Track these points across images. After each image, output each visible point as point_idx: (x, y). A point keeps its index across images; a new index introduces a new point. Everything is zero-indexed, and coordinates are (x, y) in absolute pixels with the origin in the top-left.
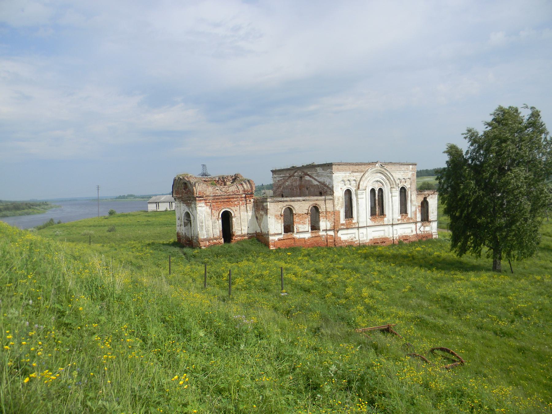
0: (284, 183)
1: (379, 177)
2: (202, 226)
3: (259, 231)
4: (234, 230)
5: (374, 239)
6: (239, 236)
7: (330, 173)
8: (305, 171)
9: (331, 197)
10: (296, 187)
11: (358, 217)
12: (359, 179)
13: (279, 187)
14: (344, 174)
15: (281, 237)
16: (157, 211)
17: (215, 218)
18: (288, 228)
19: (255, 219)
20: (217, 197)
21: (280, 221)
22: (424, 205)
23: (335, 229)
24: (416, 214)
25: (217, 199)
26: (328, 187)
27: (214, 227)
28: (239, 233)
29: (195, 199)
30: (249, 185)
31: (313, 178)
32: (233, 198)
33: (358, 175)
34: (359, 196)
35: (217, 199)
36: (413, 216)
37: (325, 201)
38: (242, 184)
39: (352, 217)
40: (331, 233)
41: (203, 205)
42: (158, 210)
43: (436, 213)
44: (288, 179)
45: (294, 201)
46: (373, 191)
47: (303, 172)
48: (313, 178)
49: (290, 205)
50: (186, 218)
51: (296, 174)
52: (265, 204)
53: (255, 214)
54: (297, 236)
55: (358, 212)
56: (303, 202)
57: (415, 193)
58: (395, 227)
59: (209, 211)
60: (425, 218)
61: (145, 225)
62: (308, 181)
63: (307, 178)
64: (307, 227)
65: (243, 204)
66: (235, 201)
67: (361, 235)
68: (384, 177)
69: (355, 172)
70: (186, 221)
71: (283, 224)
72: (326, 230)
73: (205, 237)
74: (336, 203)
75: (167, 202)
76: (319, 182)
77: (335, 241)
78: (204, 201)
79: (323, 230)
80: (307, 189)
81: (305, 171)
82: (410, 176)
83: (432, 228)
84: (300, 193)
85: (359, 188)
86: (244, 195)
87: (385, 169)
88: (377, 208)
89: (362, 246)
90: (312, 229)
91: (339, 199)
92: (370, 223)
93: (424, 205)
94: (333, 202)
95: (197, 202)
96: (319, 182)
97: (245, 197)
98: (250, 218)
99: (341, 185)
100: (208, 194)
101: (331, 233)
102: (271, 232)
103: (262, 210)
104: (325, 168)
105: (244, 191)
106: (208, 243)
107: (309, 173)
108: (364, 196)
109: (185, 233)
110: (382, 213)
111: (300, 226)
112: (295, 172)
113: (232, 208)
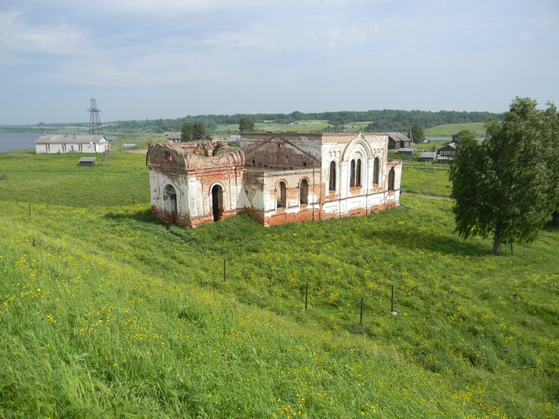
1: (359, 148)
2: (194, 203)
3: (249, 205)
4: (224, 206)
5: (352, 211)
6: (229, 211)
7: (318, 144)
8: (286, 138)
9: (318, 170)
10: (272, 154)
11: (340, 189)
12: (343, 151)
13: (251, 151)
14: (331, 146)
15: (274, 213)
16: (47, 154)
18: (281, 204)
19: (245, 193)
20: (208, 170)
22: (392, 173)
23: (321, 202)
24: (385, 184)
25: (209, 172)
26: (314, 158)
29: (185, 173)
30: (239, 157)
31: (295, 147)
32: (223, 171)
33: (343, 146)
34: (342, 168)
35: (209, 172)
36: (383, 186)
37: (314, 173)
38: (232, 155)
39: (334, 189)
40: (317, 206)
41: (194, 179)
42: (49, 152)
43: (399, 183)
44: (262, 145)
46: (353, 161)
47: (283, 139)
48: (295, 147)
49: (284, 180)
52: (260, 179)
53: (245, 187)
54: (288, 211)
56: (295, 175)
57: (385, 163)
59: (200, 185)
60: (391, 188)
61: (39, 171)
62: (289, 149)
63: (288, 146)
67: (342, 208)
69: (340, 143)
70: (165, 194)
71: (276, 200)
73: (196, 215)
74: (323, 176)
75: (59, 143)
77: (320, 214)
78: (195, 175)
79: (310, 204)
80: (287, 157)
81: (286, 138)
82: (383, 146)
83: (395, 197)
85: (343, 160)
86: (234, 168)
87: (365, 140)
88: (356, 179)
89: (344, 219)
91: (325, 171)
92: (350, 195)
93: (392, 173)
94: (321, 175)
95: (189, 176)
97: (235, 170)
98: (239, 192)
99: (328, 156)
100: (199, 166)
101: (317, 206)
102: (266, 209)
103: (254, 184)
104: (312, 138)
105: (234, 162)
106: (198, 222)
107: (290, 141)
108: (346, 168)
110: (359, 184)
111: (291, 200)
112: (272, 138)
113: (222, 182)
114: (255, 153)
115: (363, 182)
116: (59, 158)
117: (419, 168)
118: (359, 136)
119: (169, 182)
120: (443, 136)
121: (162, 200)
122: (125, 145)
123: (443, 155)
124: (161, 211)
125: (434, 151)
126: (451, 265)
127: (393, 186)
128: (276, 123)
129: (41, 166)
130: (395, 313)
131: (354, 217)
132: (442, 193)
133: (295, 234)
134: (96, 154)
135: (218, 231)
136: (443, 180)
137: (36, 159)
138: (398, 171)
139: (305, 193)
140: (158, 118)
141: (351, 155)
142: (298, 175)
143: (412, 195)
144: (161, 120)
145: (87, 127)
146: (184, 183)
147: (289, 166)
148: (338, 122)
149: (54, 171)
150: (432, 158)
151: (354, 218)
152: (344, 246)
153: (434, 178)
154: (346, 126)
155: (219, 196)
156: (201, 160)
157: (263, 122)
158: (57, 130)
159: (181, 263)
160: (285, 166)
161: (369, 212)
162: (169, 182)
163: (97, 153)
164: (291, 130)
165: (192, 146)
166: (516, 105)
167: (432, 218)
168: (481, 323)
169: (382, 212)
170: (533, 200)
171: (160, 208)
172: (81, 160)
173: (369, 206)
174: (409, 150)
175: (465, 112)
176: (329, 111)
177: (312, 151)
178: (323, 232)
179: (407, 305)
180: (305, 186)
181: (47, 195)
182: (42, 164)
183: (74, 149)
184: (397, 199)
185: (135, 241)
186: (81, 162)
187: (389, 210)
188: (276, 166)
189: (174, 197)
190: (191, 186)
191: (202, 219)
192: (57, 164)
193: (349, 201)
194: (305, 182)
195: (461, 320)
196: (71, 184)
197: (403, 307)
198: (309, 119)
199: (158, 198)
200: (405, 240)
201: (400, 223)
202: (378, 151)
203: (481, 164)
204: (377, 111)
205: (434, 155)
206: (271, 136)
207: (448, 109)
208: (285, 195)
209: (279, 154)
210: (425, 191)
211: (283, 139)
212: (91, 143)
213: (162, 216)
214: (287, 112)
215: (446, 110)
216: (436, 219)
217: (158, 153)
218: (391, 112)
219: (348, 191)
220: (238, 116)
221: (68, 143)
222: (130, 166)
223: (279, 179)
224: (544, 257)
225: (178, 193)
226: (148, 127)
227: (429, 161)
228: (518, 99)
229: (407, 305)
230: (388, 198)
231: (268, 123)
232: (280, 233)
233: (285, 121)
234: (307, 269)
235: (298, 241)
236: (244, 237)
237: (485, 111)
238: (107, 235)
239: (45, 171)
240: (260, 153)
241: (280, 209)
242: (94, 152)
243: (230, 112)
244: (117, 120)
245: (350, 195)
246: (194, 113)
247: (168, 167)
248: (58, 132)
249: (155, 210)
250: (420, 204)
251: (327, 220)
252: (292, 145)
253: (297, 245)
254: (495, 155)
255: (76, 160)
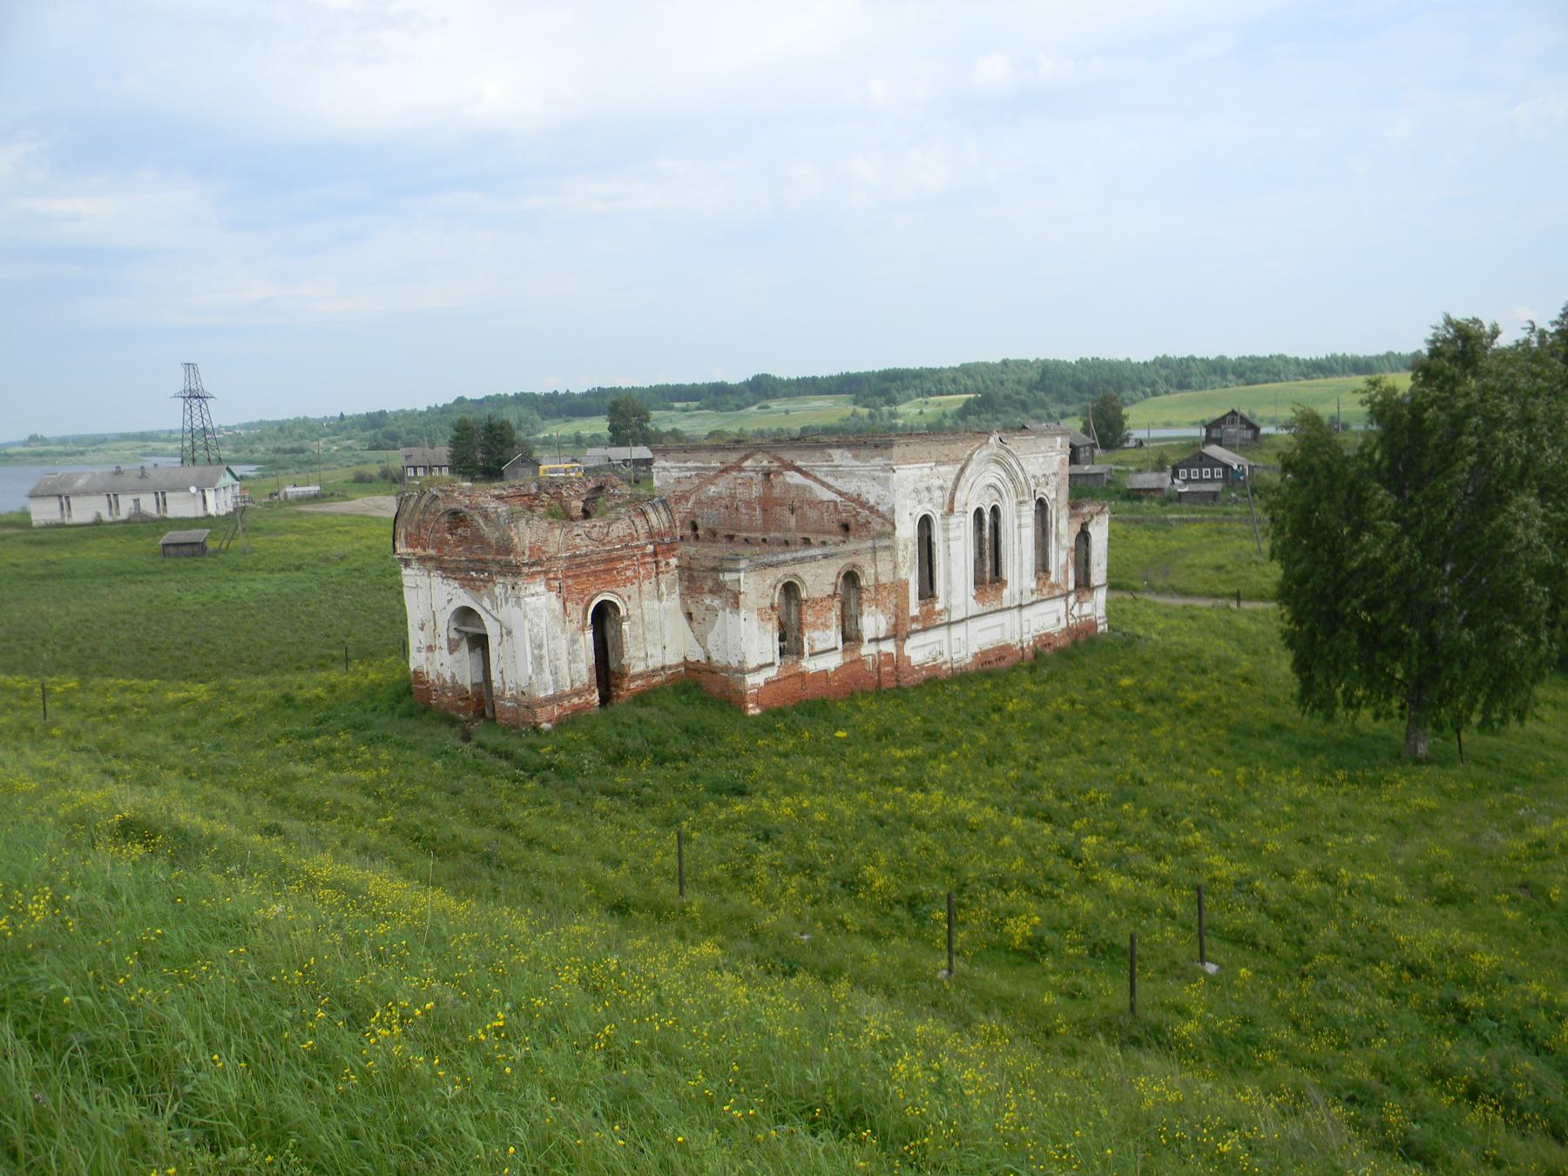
0: (698, 489)
1: (993, 474)
2: (541, 657)
3: (696, 655)
6: (639, 676)
7: (883, 470)
10: (748, 504)
11: (948, 594)
12: (950, 484)
15: (771, 673)
17: (574, 626)
18: (790, 641)
20: (578, 561)
21: (769, 626)
23: (898, 633)
24: (1066, 572)
26: (871, 509)
27: (573, 657)
28: (638, 667)
30: (664, 515)
31: (815, 479)
32: (621, 558)
33: (949, 471)
34: (952, 535)
35: (581, 565)
36: (1061, 577)
38: (644, 513)
40: (889, 647)
41: (541, 588)
42: (67, 521)
43: (1104, 567)
44: (716, 477)
45: (801, 561)
46: (979, 513)
47: (779, 459)
50: (453, 625)
51: (748, 463)
52: (728, 577)
53: (684, 603)
54: (811, 665)
55: (948, 581)
56: (823, 562)
57: (1065, 512)
58: (1026, 612)
59: (557, 605)
60: (1084, 584)
61: (43, 577)
62: (797, 486)
63: (794, 478)
64: (833, 637)
65: (648, 576)
66: (626, 569)
67: (955, 644)
68: (1003, 474)
69: (944, 464)
70: (454, 635)
72: (877, 640)
73: (551, 692)
75: (98, 493)
76: (840, 494)
77: (897, 668)
80: (793, 511)
81: (787, 456)
83: (1096, 607)
84: (765, 521)
85: (951, 510)
86: (650, 548)
87: (1008, 451)
88: (988, 563)
89: (962, 677)
90: (845, 640)
91: (906, 547)
92: (975, 608)
93: (1083, 537)
96: (840, 494)
97: (655, 554)
100: (552, 549)
101: (889, 647)
103: (711, 592)
104: (864, 452)
105: (651, 534)
107: (799, 463)
108: (960, 532)
109: (453, 676)
111: (816, 635)
112: (746, 458)
114: (699, 503)
115: (1009, 570)
116: (99, 537)
117: (1130, 520)
118: (991, 440)
119: (464, 599)
120: (1168, 425)
121: (445, 651)
122: (290, 489)
123: (1187, 481)
124: (443, 687)
125: (1163, 470)
126: (1312, 803)
127: (1087, 575)
128: (707, 408)
129: (47, 563)
130: (1211, 968)
131: (994, 670)
132: (1207, 587)
133: (840, 734)
134: (207, 521)
135: (620, 735)
136: (1249, 551)
137: (31, 543)
138: (1099, 533)
139: (853, 612)
140: (374, 408)
141: (972, 497)
142: (831, 561)
143: (1128, 596)
144: (382, 414)
145: (169, 441)
146: (512, 601)
147: (800, 535)
148: (879, 400)
149: (87, 575)
150: (1160, 490)
151: (989, 675)
152: (990, 763)
153: (1175, 544)
154: (901, 409)
155: (610, 633)
156: (558, 532)
157: (671, 409)
158: (82, 453)
159: (530, 843)
160: (789, 536)
161: (1029, 654)
162: (464, 599)
163: (209, 516)
164: (751, 427)
165: (524, 490)
166: (1445, 341)
167: (1207, 661)
168: (1468, 982)
169: (1062, 653)
170: (1510, 602)
171: (439, 675)
172: (164, 540)
173: (1028, 640)
174: (1096, 469)
175: (1222, 358)
176: (853, 371)
177: (864, 490)
178: (916, 721)
179: (1240, 939)
180: (853, 592)
181: (74, 649)
182: (52, 557)
183: (143, 507)
184: (1101, 612)
185: (379, 780)
186: (165, 545)
187: (1081, 641)
188: (760, 536)
189: (479, 642)
190: (533, 609)
191: (566, 703)
192: (95, 553)
193: (973, 625)
194: (851, 578)
195: (1406, 975)
196: (143, 611)
197: (1227, 946)
198: (799, 394)
199: (430, 649)
200: (1154, 732)
201: (1126, 681)
202: (1043, 480)
203: (1357, 501)
204: (985, 364)
205: (1164, 480)
206: (743, 453)
207: (1178, 351)
208: (800, 619)
209: (767, 503)
210: (1159, 582)
211: (779, 459)
212: (193, 489)
213: (445, 700)
214: (736, 376)
215: (1171, 354)
216: (1219, 663)
217: (428, 517)
218: (1023, 365)
219: (971, 599)
220: (601, 393)
221: (124, 492)
222: (310, 549)
223: (781, 574)
224: (1546, 759)
225: (492, 630)
226: (344, 434)
227: (1152, 499)
228: (1449, 322)
229: (1240, 939)
230: (1076, 612)
231: (685, 410)
232: (793, 731)
233: (733, 401)
234: (915, 841)
235: (855, 754)
236: (697, 750)
237: (1276, 353)
238: (291, 767)
239: (60, 576)
240: (712, 501)
241: (790, 660)
242: (201, 513)
243: (579, 383)
244: (256, 419)
245: (975, 608)
246: (476, 391)
247: (460, 554)
248: (86, 458)
249: (422, 683)
250: (1164, 619)
251: (917, 687)
252: (806, 474)
253: (855, 767)
254: (1394, 482)
255: (150, 540)
